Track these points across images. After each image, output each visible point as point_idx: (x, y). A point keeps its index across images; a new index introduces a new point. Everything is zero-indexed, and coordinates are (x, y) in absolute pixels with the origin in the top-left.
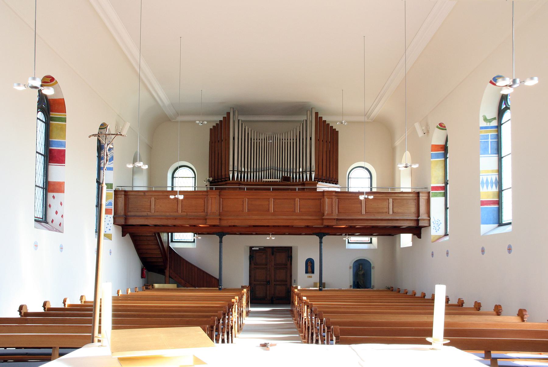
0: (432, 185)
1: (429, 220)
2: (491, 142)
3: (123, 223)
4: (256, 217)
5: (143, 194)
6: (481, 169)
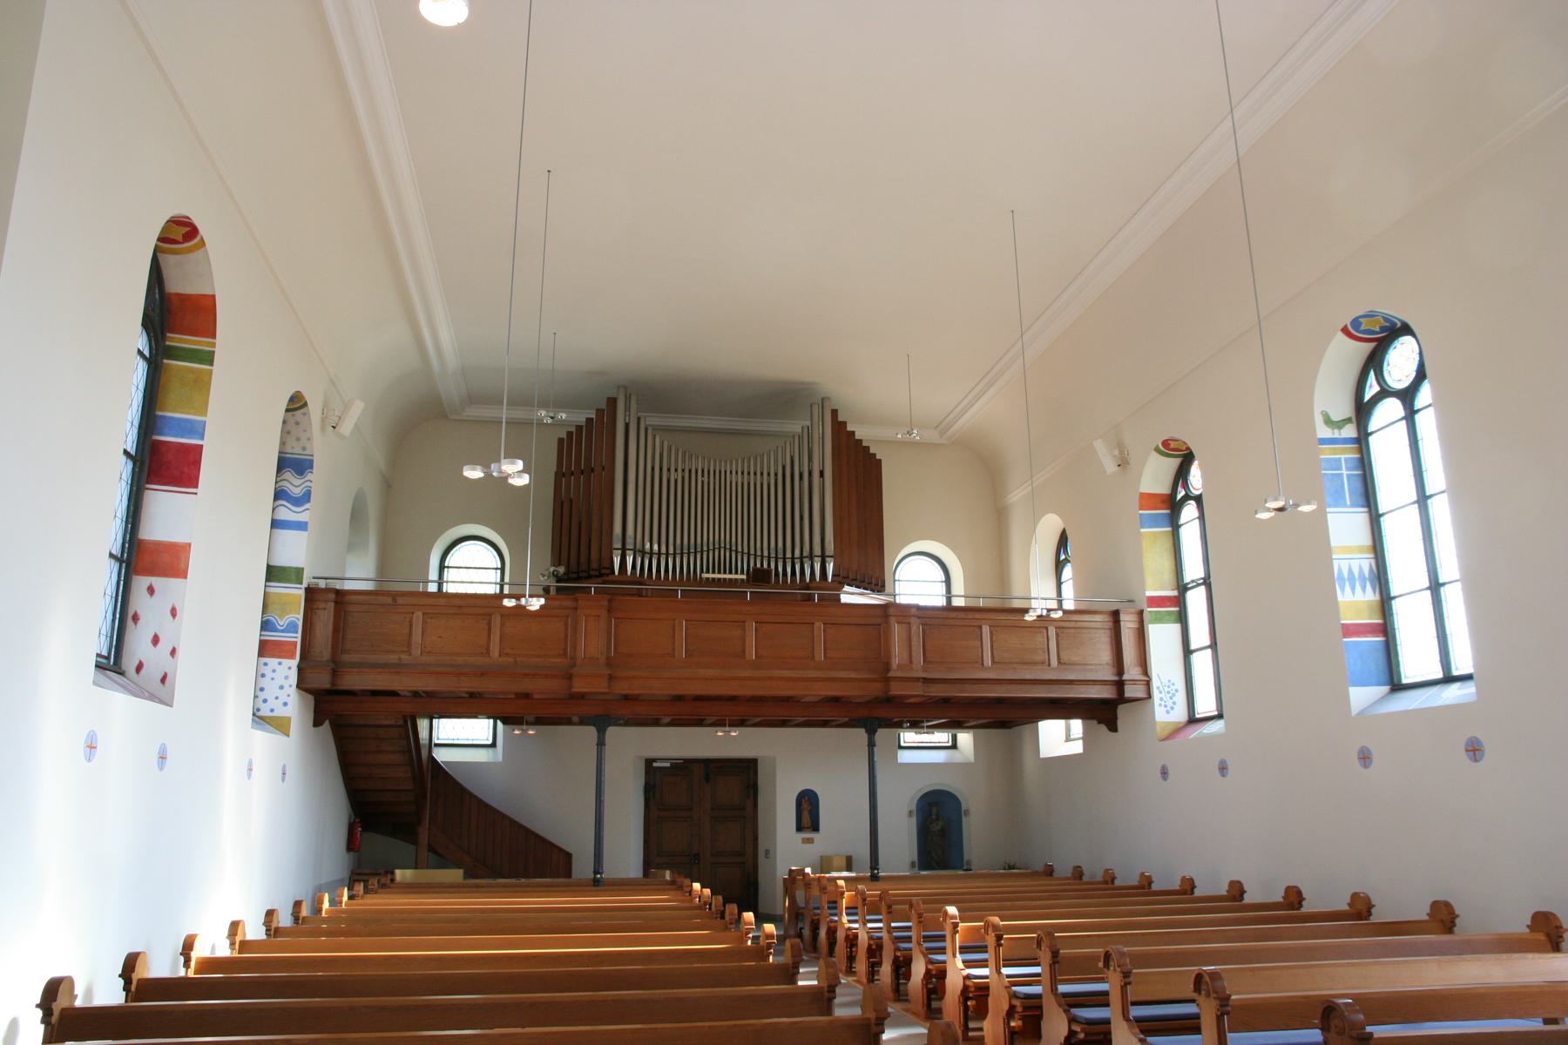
0: (1149, 593)
1: (1148, 684)
3: (328, 686)
4: (711, 672)
5: (389, 600)
6: (1334, 543)
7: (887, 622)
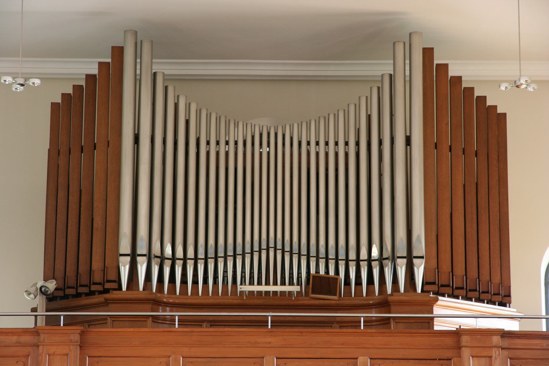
7: (459, 356)
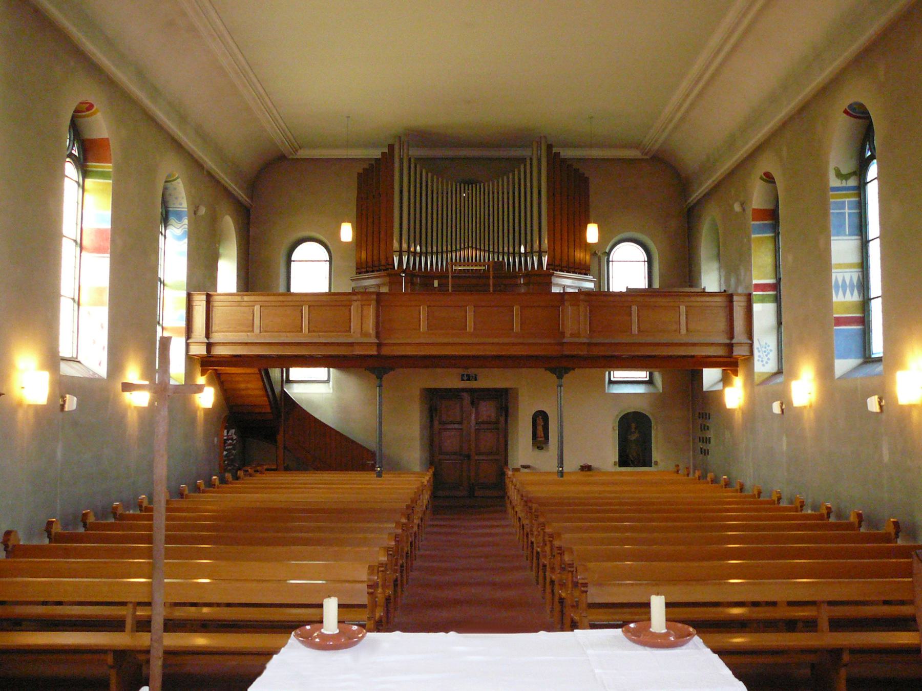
0: (755, 282)
1: (751, 346)
2: (849, 214)
